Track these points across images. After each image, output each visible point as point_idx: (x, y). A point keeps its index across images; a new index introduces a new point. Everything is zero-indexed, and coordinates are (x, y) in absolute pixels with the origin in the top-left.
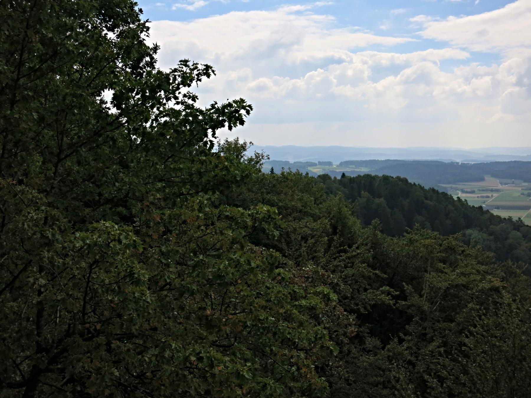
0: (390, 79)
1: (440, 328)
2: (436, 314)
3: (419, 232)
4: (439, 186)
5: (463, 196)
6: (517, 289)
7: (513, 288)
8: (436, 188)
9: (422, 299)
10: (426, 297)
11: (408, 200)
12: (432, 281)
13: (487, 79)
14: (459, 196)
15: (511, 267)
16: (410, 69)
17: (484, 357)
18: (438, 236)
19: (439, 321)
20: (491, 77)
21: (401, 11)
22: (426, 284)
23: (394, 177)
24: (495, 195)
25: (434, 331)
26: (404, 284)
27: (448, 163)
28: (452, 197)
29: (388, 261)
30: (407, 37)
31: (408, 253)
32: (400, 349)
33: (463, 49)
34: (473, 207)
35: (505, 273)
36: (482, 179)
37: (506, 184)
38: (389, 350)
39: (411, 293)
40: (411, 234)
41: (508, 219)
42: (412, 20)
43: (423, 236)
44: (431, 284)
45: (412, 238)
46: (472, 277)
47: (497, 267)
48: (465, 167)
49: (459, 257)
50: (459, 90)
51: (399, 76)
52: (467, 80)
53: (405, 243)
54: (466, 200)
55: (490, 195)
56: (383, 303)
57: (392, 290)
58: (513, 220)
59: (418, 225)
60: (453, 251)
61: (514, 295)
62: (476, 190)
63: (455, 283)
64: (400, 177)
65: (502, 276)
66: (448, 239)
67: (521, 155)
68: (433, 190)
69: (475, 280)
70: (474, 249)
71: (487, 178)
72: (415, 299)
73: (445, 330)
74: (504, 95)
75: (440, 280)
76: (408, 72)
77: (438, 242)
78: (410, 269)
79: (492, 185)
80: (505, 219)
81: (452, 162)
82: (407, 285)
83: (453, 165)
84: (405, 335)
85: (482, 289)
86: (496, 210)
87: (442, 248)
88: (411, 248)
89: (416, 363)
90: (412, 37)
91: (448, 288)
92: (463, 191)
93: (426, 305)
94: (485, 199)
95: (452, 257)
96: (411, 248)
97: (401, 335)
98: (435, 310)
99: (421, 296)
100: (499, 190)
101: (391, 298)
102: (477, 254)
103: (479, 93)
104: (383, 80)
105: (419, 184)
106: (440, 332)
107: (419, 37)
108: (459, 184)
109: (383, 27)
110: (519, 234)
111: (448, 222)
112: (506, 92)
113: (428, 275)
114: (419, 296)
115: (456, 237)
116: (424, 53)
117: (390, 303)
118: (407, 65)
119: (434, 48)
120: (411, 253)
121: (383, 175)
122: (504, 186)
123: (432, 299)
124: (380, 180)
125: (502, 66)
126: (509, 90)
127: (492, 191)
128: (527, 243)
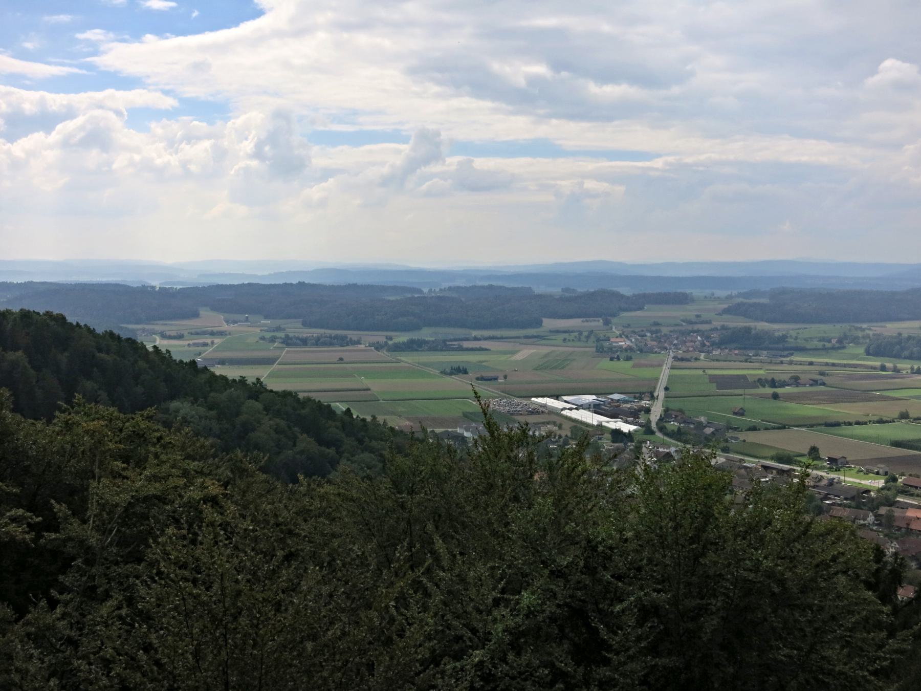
0: (35, 139)
1: (119, 574)
2: (112, 551)
3: (82, 408)
4: (122, 328)
5: (163, 344)
6: (250, 497)
7: (244, 496)
8: (116, 332)
9: (85, 526)
10: (94, 522)
11: (66, 354)
12: (103, 494)
13: (207, 144)
14: (157, 343)
15: (241, 461)
16: (75, 121)
17: (174, 617)
18: (116, 414)
19: (117, 563)
20: (213, 141)
21: (64, 18)
22: (93, 499)
23: (41, 314)
24: (218, 341)
25: (110, 580)
26: (53, 501)
27: (137, 287)
28: (144, 347)
29: (26, 463)
30: (70, 65)
31: (62, 446)
32: (49, 619)
33: (167, 93)
34: (181, 362)
35: (232, 471)
36: (196, 315)
37: (235, 322)
38: (28, 623)
39: (66, 519)
40: (67, 413)
41: (240, 381)
42: (80, 36)
43: (89, 416)
44: (102, 498)
45: (70, 419)
46: (172, 482)
47: (219, 462)
48: (166, 294)
49: (153, 449)
50: (158, 162)
51: (54, 133)
52: (172, 144)
53: (57, 429)
54: (168, 351)
55: (209, 341)
56: (13, 539)
57: (29, 514)
58: (248, 382)
59: (80, 397)
60: (142, 439)
61: (245, 507)
62: (186, 333)
63: (143, 494)
64: (52, 312)
65: (227, 476)
66: (133, 419)
67: (259, 273)
68: (111, 334)
69: (176, 487)
70: (179, 434)
71: (203, 312)
72: (74, 528)
73: (127, 577)
74: (232, 172)
75: (116, 491)
76: (69, 126)
77: (116, 424)
78: (67, 475)
79: (211, 325)
80: (234, 381)
81: (144, 286)
82: (58, 502)
83: (145, 291)
84: (61, 593)
85: (189, 502)
86: (219, 366)
87: (123, 435)
88: (68, 438)
89: (79, 640)
90: (80, 66)
91: (130, 503)
92: (164, 336)
93: (93, 537)
94: (200, 349)
95: (142, 451)
96: (68, 438)
97: (54, 593)
98: (109, 543)
99: (84, 522)
100: (223, 332)
101: (27, 529)
102: (184, 443)
103: (193, 168)
104: (25, 139)
105: (85, 325)
106: (119, 582)
107: (91, 67)
108: (157, 324)
109: (29, 45)
110: (258, 406)
111: (139, 389)
112: (236, 167)
113: (95, 484)
114: (80, 522)
115: (148, 414)
116: (98, 95)
117: (24, 539)
118: (69, 114)
119: (118, 89)
120: (68, 447)
121: (21, 310)
122: (232, 325)
123: (104, 524)
124: (15, 319)
125: (230, 124)
126: (242, 164)
127: (212, 334)
128: (270, 420)
